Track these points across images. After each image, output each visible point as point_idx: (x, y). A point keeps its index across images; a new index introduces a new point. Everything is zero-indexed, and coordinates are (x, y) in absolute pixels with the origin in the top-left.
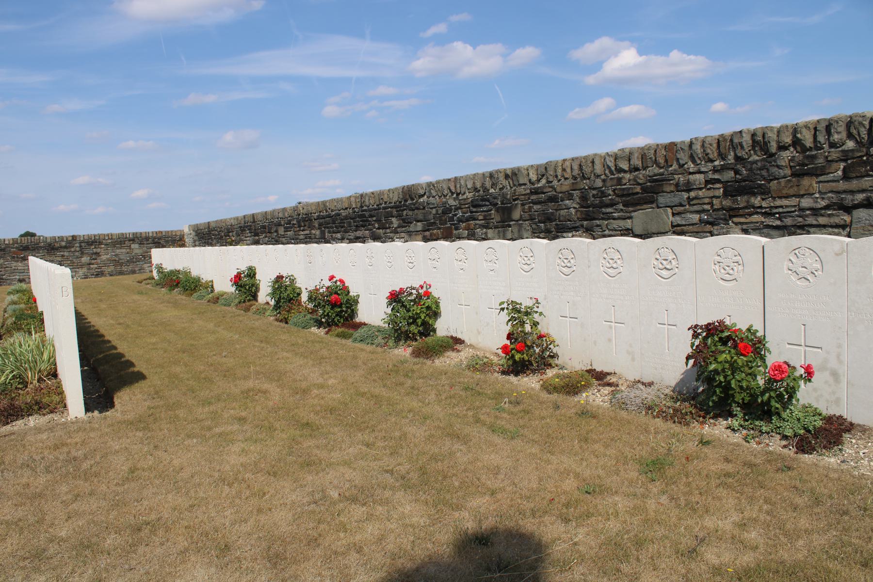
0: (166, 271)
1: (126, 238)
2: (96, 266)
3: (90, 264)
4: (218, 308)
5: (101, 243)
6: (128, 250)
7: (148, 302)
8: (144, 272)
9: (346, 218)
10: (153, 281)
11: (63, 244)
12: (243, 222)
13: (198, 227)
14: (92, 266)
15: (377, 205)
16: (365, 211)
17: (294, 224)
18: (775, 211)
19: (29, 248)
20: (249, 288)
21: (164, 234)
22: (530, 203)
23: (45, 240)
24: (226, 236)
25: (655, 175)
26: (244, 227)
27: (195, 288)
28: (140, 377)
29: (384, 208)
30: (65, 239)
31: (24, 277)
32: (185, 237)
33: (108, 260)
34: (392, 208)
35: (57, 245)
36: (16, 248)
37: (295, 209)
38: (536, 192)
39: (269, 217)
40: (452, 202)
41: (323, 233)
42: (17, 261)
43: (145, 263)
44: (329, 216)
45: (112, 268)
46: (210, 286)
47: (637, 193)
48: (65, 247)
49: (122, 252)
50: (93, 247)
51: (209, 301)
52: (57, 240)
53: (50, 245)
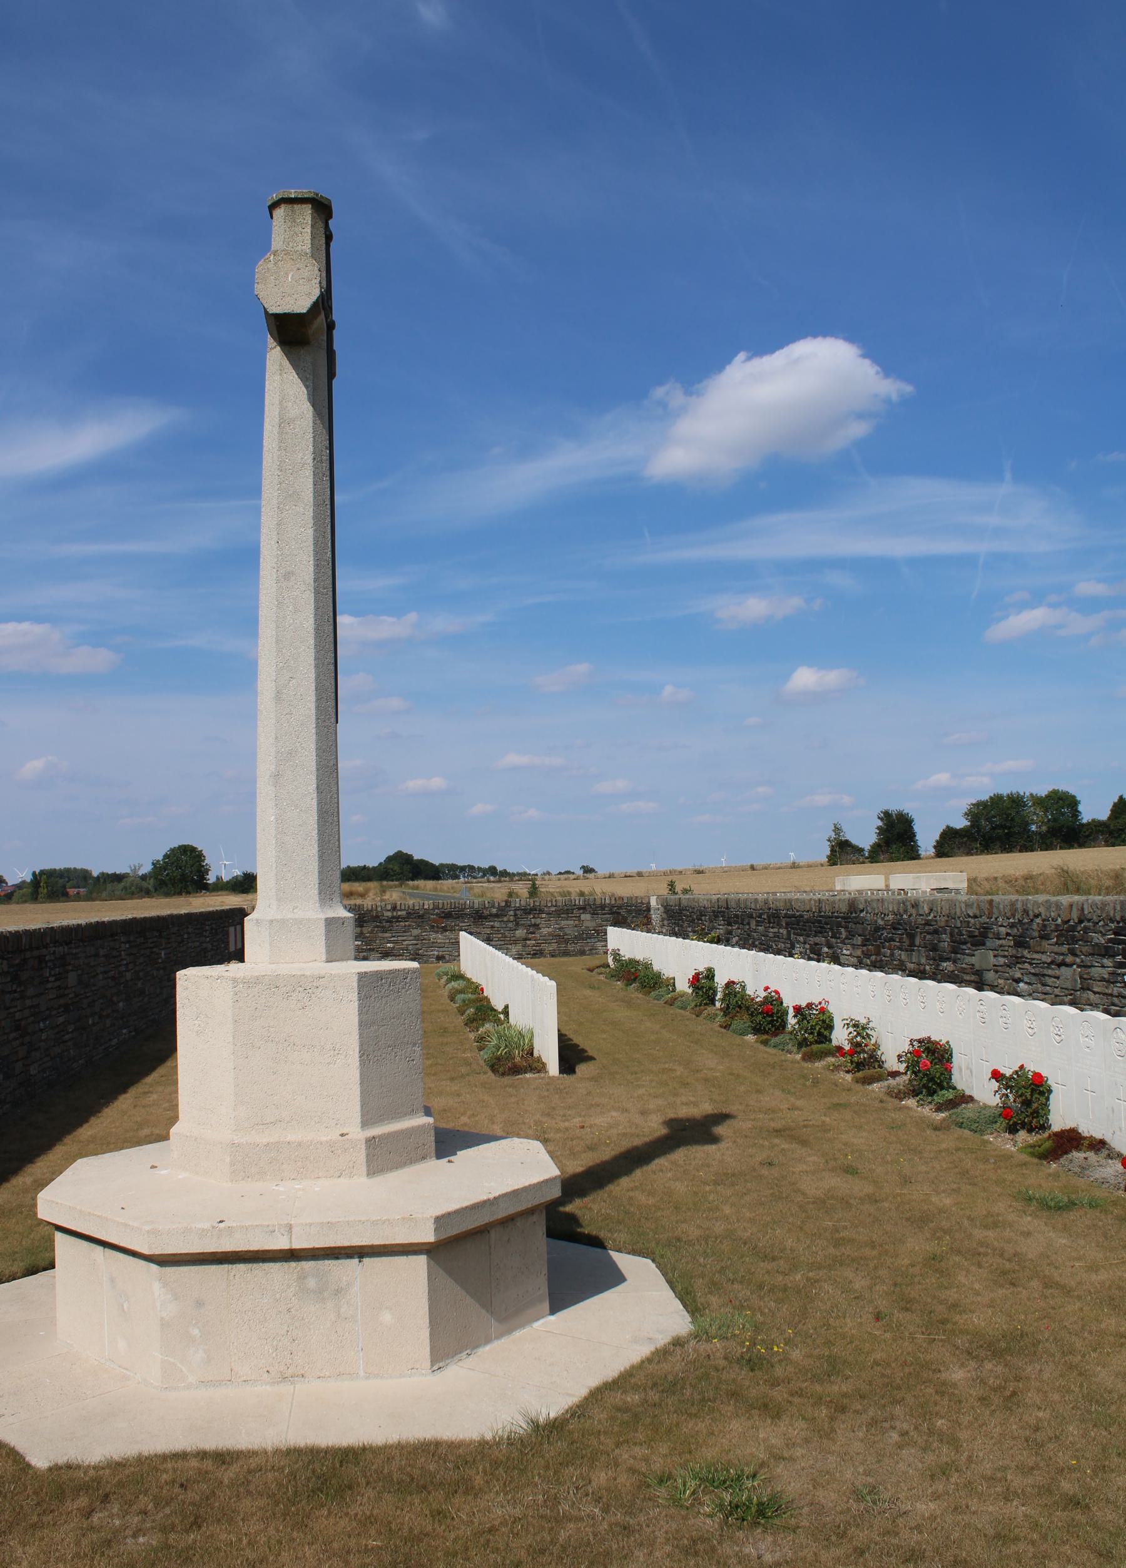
0: (624, 959)
1: (575, 905)
2: (534, 942)
3: (526, 939)
4: (672, 1010)
5: (541, 911)
6: (577, 922)
7: (600, 999)
8: (596, 954)
9: (808, 921)
10: (608, 970)
11: (494, 911)
12: (716, 907)
13: (667, 901)
14: (528, 942)
15: (832, 913)
16: (821, 916)
17: (765, 919)
18: (1033, 962)
19: (451, 914)
20: (706, 990)
21: (625, 901)
22: (925, 932)
23: (471, 905)
24: (698, 920)
25: (985, 923)
26: (718, 912)
27: (654, 986)
28: (591, 1058)
29: (837, 917)
30: (497, 905)
31: (444, 953)
32: (652, 912)
33: (550, 934)
34: (842, 917)
35: (486, 912)
36: (437, 914)
37: (766, 902)
38: (928, 923)
39: (742, 906)
40: (881, 922)
41: (789, 933)
42: (437, 932)
43: (599, 941)
44: (793, 916)
45: (555, 946)
46: (671, 983)
47: (977, 936)
48: (497, 916)
49: (568, 924)
50: (532, 916)
51: (665, 1003)
52: (487, 906)
53: (477, 912)
